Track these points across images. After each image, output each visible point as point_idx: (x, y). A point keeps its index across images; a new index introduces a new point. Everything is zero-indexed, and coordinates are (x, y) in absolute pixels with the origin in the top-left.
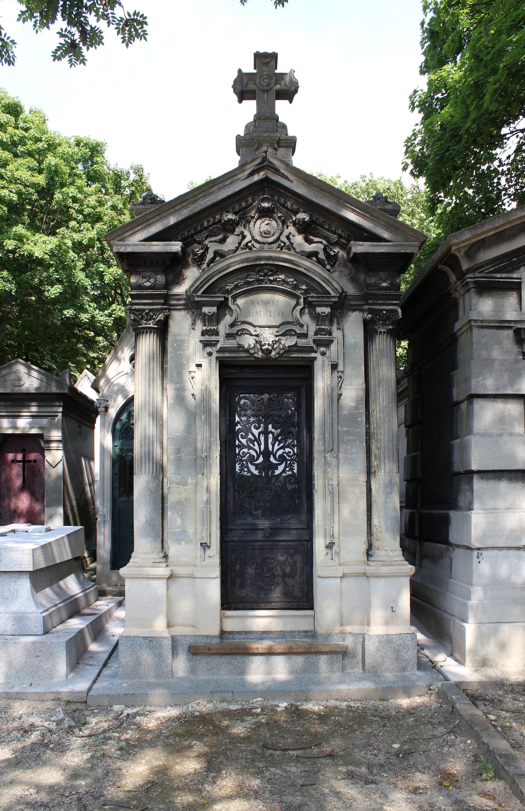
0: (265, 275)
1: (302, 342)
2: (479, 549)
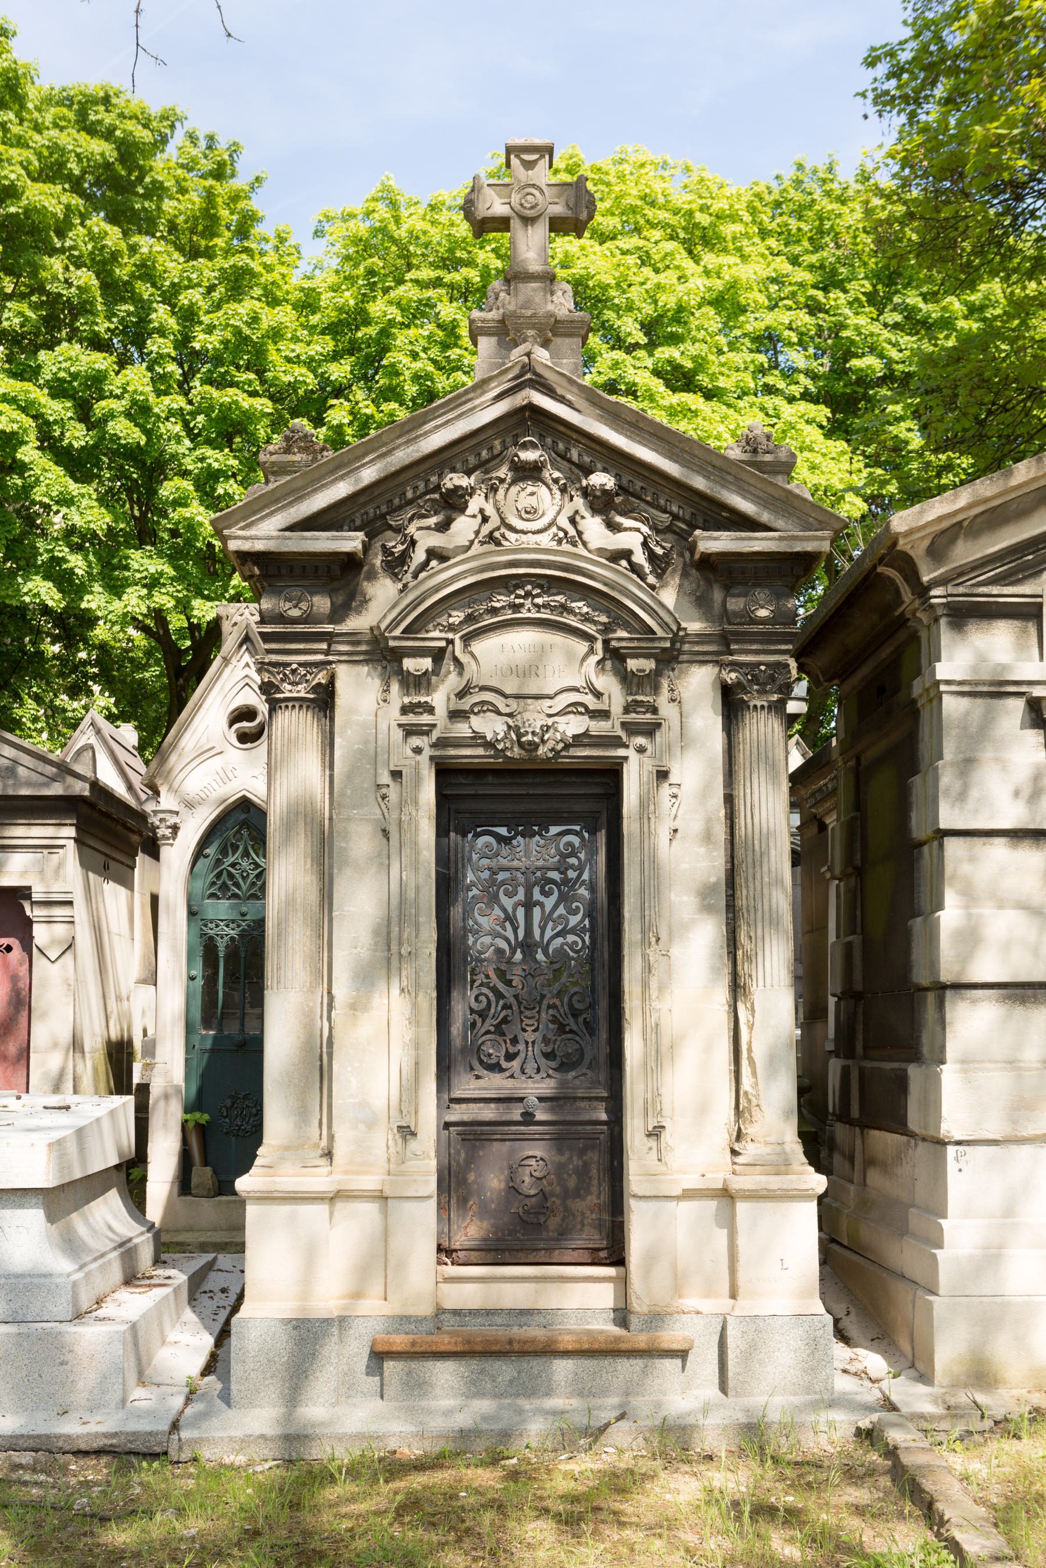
0: (528, 595)
1: (599, 727)
2: (959, 1143)
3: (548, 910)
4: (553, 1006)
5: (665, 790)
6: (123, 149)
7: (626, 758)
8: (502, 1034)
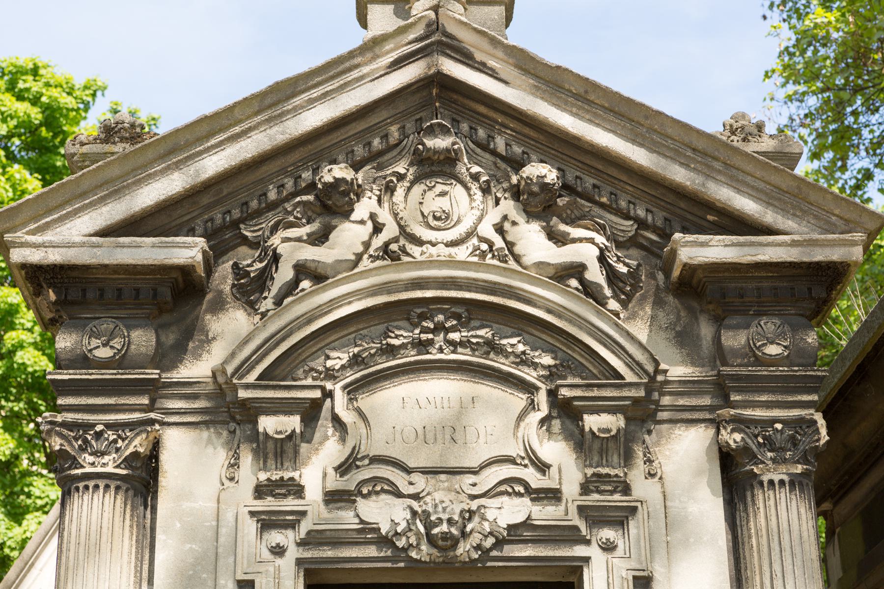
0: (439, 328)
1: (545, 514)
6: (48, 112)
7: (587, 560)
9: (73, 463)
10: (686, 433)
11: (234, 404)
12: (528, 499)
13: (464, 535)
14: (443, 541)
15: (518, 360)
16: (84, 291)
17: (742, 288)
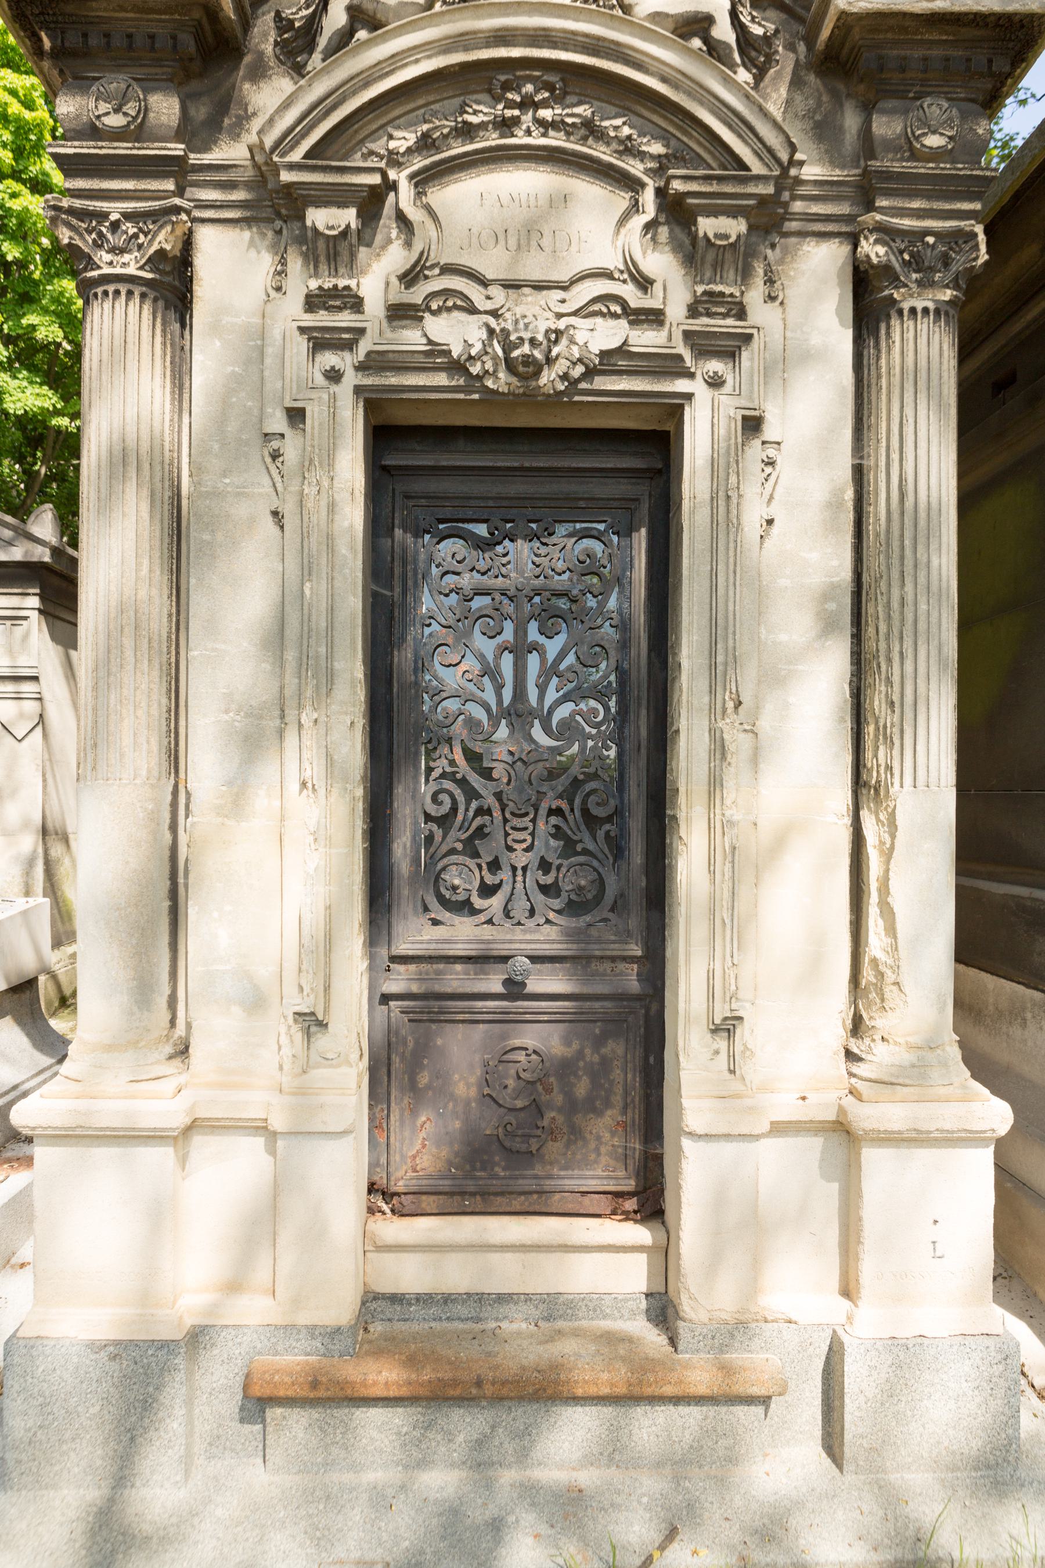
0: (527, 104)
1: (646, 340)
3: (551, 656)
4: (558, 812)
5: (755, 451)
7: (689, 396)
8: (476, 855)
9: (88, 263)
10: (816, 250)
11: (277, 192)
12: (625, 321)
13: (550, 361)
14: (524, 366)
15: (621, 148)
16: (85, 35)
17: (905, 58)
